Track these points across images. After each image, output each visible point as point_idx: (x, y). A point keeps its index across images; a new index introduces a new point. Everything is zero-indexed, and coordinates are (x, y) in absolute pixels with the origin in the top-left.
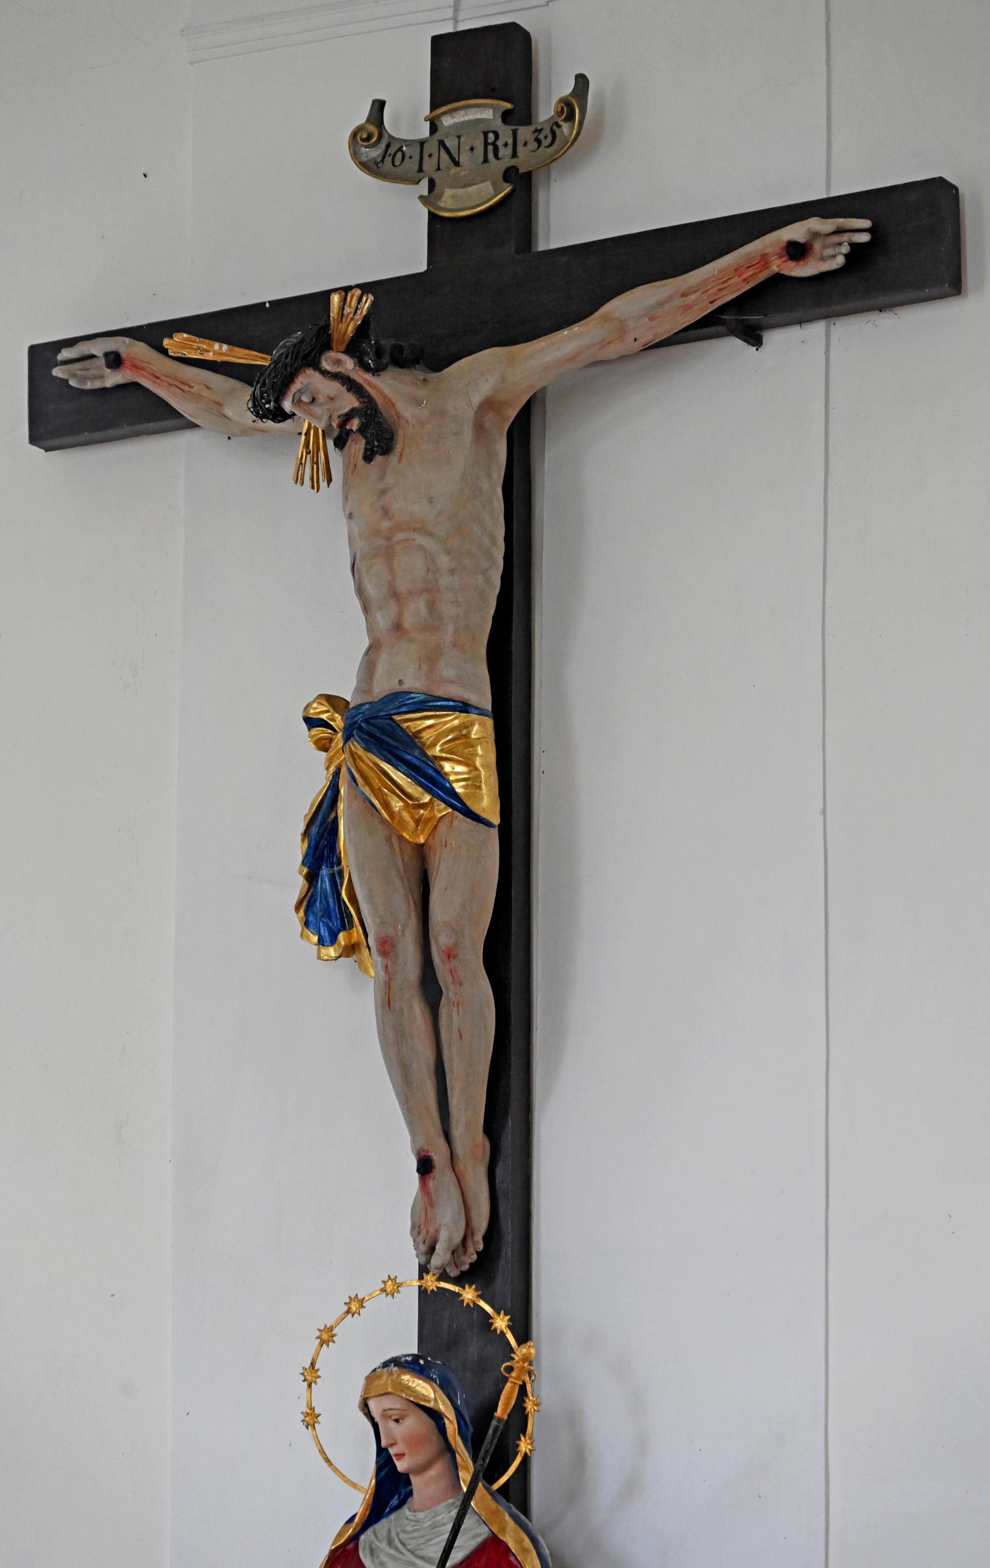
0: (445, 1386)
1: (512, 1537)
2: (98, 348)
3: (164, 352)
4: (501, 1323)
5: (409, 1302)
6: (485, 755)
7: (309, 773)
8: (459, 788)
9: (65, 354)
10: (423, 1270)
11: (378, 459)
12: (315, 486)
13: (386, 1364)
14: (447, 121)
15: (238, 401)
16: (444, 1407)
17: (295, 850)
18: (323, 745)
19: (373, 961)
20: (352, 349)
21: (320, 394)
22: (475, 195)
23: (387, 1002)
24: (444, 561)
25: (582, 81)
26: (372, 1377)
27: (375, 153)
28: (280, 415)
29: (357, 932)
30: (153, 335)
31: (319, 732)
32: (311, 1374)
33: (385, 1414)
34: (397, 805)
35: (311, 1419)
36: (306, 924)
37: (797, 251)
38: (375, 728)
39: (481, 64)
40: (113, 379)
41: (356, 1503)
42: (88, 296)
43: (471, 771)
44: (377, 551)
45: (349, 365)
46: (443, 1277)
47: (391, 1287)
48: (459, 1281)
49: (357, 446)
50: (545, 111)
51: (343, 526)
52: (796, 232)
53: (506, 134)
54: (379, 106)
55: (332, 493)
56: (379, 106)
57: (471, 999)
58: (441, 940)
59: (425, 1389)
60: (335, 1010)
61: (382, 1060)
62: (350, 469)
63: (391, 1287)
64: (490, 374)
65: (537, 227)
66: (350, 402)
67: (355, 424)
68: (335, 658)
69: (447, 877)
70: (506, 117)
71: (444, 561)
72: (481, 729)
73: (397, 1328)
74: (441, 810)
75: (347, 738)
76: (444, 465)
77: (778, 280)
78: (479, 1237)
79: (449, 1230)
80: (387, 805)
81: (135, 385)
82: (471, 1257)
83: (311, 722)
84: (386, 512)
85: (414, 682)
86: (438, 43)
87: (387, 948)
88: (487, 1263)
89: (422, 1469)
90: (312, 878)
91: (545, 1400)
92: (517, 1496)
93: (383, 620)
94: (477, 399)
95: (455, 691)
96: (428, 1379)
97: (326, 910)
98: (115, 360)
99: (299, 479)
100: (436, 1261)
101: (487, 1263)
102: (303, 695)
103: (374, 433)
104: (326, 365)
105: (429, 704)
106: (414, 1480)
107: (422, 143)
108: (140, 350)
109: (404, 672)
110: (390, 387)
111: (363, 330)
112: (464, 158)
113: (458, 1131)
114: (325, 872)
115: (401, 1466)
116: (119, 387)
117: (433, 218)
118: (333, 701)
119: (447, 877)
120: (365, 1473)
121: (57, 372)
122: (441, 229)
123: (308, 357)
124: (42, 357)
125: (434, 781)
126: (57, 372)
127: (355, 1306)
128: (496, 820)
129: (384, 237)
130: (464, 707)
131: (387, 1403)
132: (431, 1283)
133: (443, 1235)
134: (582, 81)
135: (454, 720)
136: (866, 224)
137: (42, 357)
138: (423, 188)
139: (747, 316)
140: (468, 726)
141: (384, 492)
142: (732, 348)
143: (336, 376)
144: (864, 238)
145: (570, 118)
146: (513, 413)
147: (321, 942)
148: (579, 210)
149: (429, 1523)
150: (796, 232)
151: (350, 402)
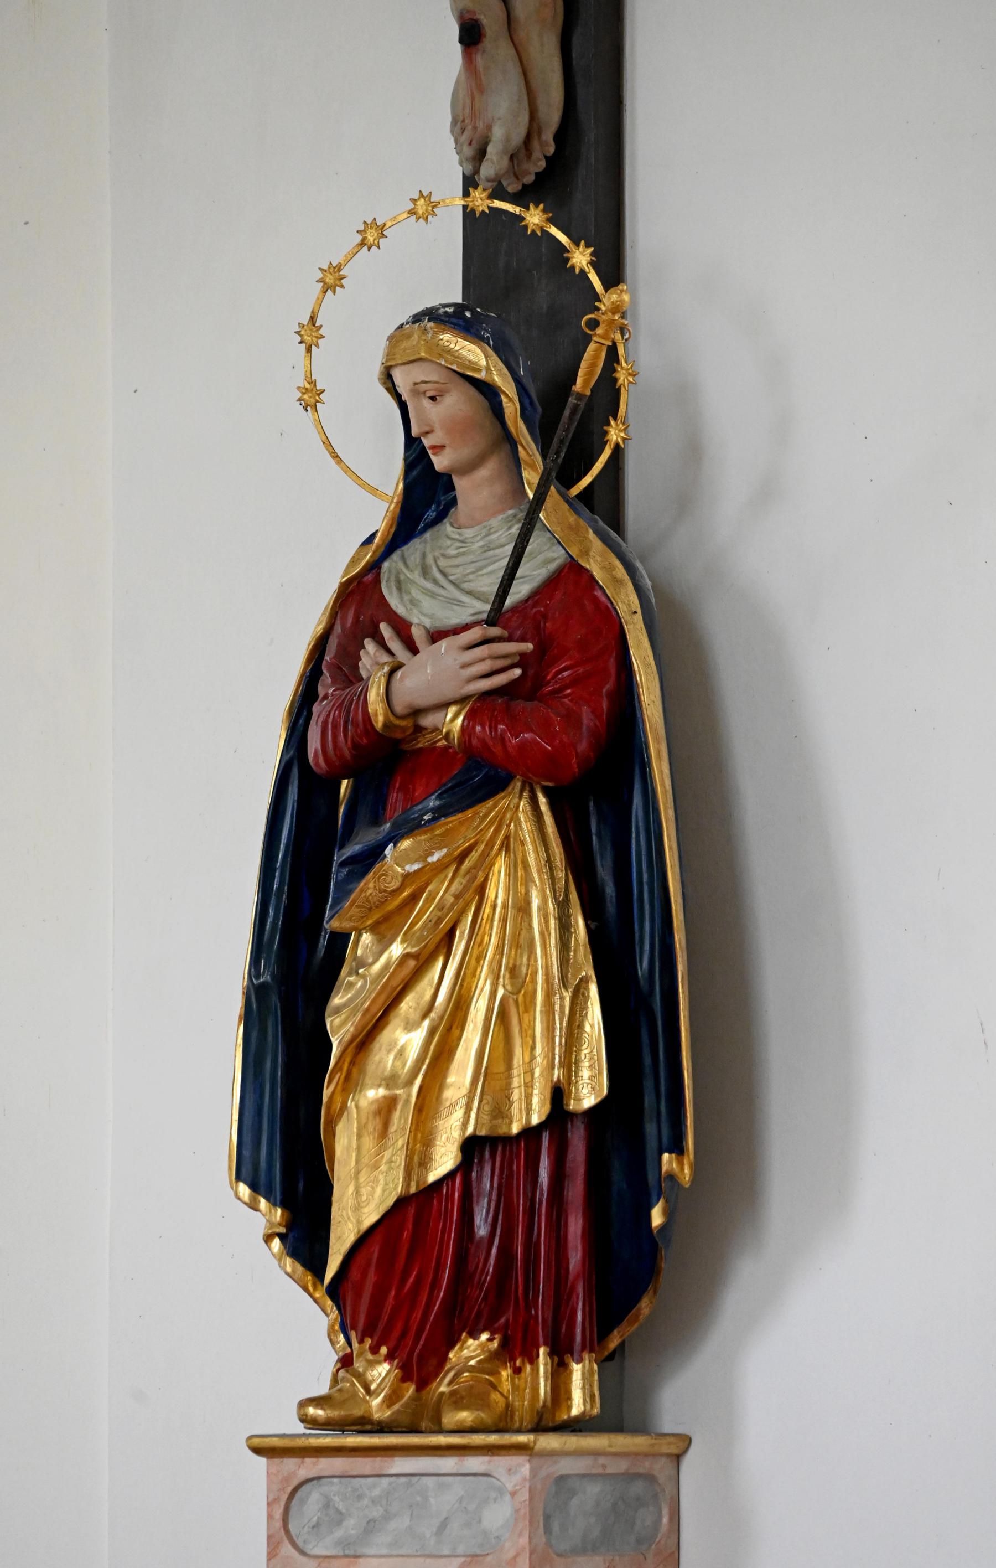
1: (599, 563)
10: (469, 183)
13: (417, 319)
16: (501, 379)
32: (310, 333)
35: (311, 397)
41: (376, 516)
46: (498, 193)
47: (422, 208)
48: (521, 198)
59: (473, 354)
63: (422, 208)
78: (548, 136)
79: (505, 121)
89: (469, 467)
91: (645, 369)
92: (605, 506)
100: (487, 170)
106: (461, 484)
115: (440, 462)
120: (389, 474)
127: (372, 235)
131: (419, 373)
132: (480, 201)
133: (498, 133)
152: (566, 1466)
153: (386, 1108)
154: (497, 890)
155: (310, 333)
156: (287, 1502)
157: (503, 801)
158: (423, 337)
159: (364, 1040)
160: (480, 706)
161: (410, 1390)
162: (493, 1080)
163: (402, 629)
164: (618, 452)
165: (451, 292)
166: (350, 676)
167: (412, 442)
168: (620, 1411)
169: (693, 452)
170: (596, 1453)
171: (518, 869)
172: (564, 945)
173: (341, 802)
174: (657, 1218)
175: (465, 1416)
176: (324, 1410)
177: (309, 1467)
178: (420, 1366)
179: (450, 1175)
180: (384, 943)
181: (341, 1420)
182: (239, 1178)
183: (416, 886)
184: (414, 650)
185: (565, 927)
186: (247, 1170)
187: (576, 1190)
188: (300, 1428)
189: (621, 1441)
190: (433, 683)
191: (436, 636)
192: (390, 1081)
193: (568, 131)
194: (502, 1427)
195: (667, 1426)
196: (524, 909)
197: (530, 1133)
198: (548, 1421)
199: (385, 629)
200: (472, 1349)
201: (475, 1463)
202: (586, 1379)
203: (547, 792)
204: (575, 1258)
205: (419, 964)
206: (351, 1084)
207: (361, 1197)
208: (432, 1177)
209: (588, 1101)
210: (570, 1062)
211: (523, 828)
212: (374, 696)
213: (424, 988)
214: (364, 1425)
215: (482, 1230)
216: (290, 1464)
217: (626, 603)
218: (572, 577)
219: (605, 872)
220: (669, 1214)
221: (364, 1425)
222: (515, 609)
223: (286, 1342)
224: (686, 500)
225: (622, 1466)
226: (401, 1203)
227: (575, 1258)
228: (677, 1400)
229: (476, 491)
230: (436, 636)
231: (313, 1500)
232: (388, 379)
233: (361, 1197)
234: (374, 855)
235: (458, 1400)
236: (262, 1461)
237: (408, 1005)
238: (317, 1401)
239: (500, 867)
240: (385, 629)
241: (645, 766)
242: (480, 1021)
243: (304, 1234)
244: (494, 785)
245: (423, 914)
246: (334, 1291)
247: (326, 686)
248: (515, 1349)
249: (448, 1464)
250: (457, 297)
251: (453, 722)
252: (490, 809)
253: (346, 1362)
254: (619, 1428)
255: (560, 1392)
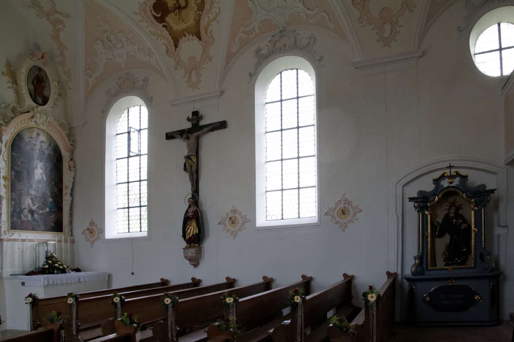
5: (191, 195)
7: (184, 161)
15: (179, 136)
21: (185, 135)
22: (195, 122)
23: (190, 175)
30: (174, 132)
38: (188, 157)
41: (187, 207)
42: (170, 130)
44: (188, 145)
57: (195, 175)
60: (186, 176)
64: (195, 134)
65: (29, 316)
68: (186, 153)
72: (195, 157)
73: (190, 196)
76: (192, 140)
79: (193, 189)
88: (196, 191)
91: (200, 200)
92: (198, 206)
97: (185, 169)
101: (196, 191)
103: (188, 138)
109: (190, 154)
120: (188, 205)
122: (193, 125)
124: (167, 134)
125: (192, 161)
129: (188, 125)
137: (167, 134)
139: (212, 130)
142: (212, 133)
148: (202, 123)
149: (69, 244)
156: (184, 251)
158: (198, 12)
162: (193, 232)
169: (202, 204)
173: (186, 220)
176: (218, 321)
178: (190, 245)
181: (186, 248)
190: (190, 214)
194: (194, 247)
207: (187, 237)
211: (194, 220)
218: (196, 210)
223: (184, 244)
224: (201, 206)
228: (201, 246)
233: (187, 237)
242: (193, 229)
243: (185, 239)
248: (194, 244)
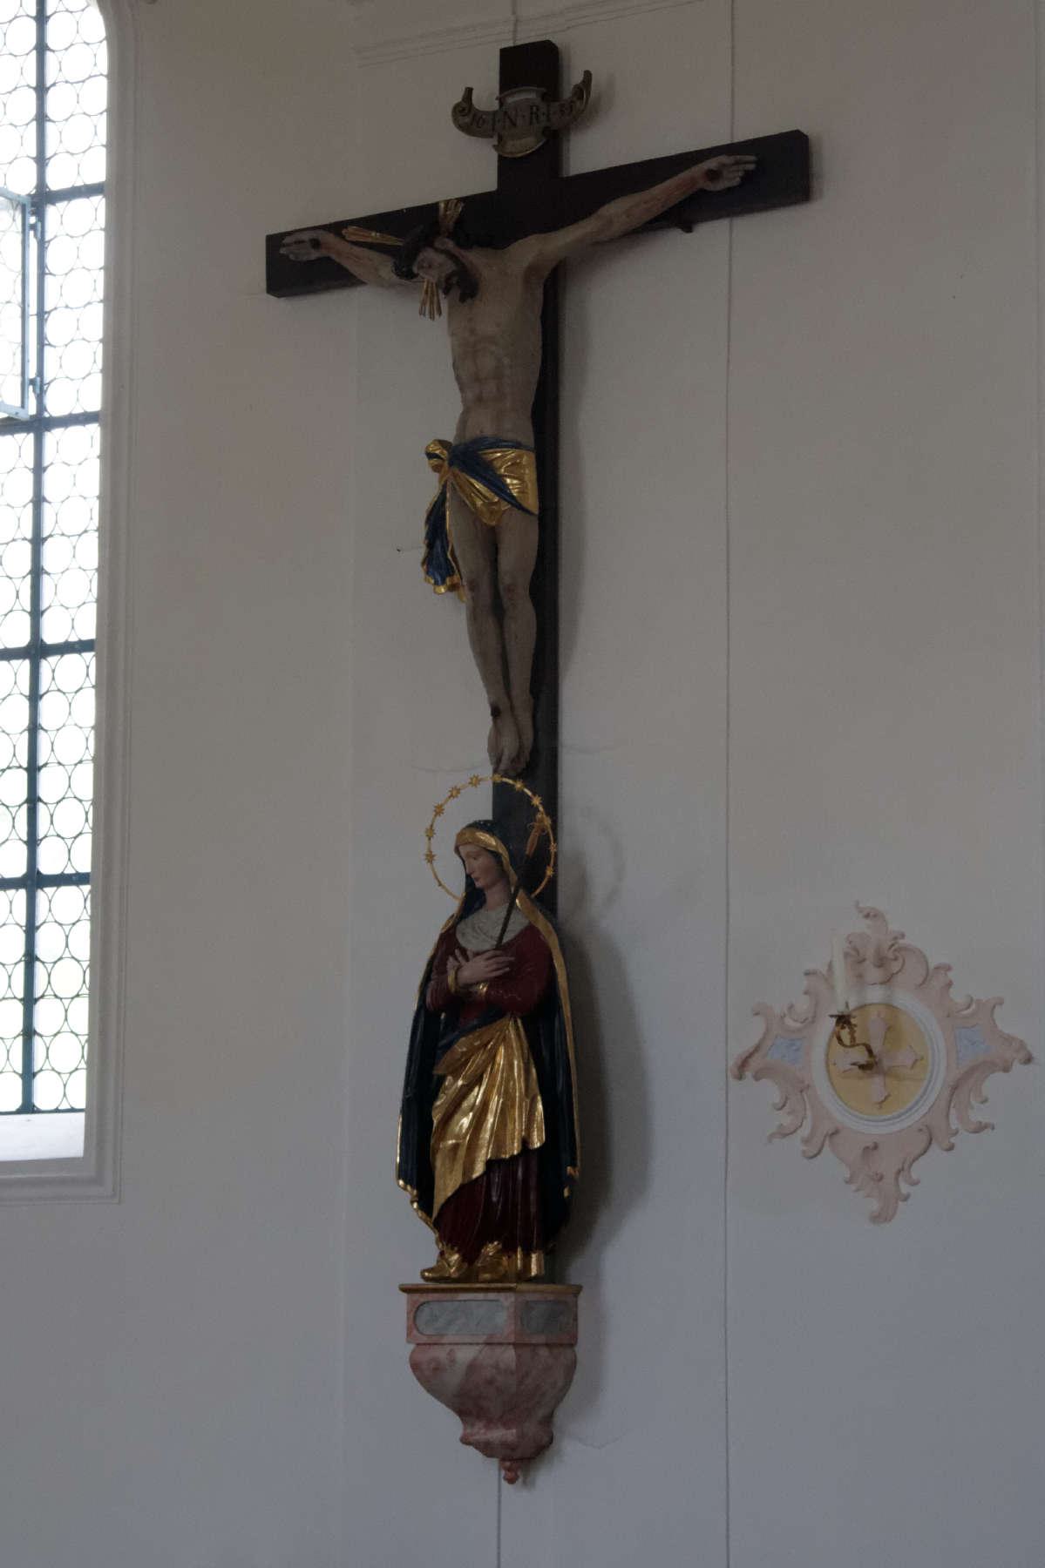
0: (504, 840)
1: (542, 924)
2: (306, 237)
3: (343, 237)
4: (536, 801)
6: (530, 474)
7: (428, 486)
8: (515, 493)
9: (287, 240)
10: (495, 771)
11: (469, 301)
12: (432, 317)
13: (470, 826)
14: (510, 100)
16: (502, 850)
17: (420, 531)
18: (436, 469)
19: (466, 593)
20: (452, 235)
21: (435, 265)
22: (524, 144)
23: (474, 617)
24: (506, 361)
25: (588, 75)
26: (460, 835)
27: (467, 120)
28: (410, 275)
29: (456, 578)
30: (337, 228)
31: (435, 461)
32: (430, 833)
33: (468, 855)
34: (479, 503)
35: (430, 857)
36: (427, 572)
37: (713, 175)
38: (464, 458)
39: (531, 65)
40: (314, 255)
41: (453, 906)
43: (521, 483)
44: (467, 354)
45: (450, 245)
46: (506, 775)
47: (475, 782)
48: (514, 779)
49: (456, 293)
50: (567, 92)
51: (458, 395)
52: (711, 164)
53: (543, 109)
54: (469, 91)
55: (443, 320)
56: (469, 91)
58: (505, 579)
59: (491, 841)
60: (445, 619)
61: (481, 683)
62: (450, 307)
63: (475, 782)
64: (531, 250)
66: (450, 267)
67: (454, 280)
69: (510, 565)
70: (544, 97)
71: (506, 361)
72: (528, 459)
73: (481, 806)
74: (505, 506)
75: (451, 465)
77: (702, 191)
78: (527, 752)
79: (509, 745)
80: (474, 504)
81: (329, 258)
82: (523, 765)
83: (430, 456)
84: (472, 331)
85: (489, 430)
86: (505, 53)
87: (473, 586)
89: (489, 887)
90: (430, 546)
91: (566, 844)
92: (547, 902)
93: (470, 395)
94: (525, 264)
95: (510, 436)
96: (493, 835)
97: (438, 563)
98: (316, 244)
99: (422, 313)
100: (502, 767)
101: (531, 759)
102: (426, 441)
103: (463, 287)
104: (437, 244)
105: (497, 444)
106: (488, 893)
107: (495, 113)
108: (330, 238)
109: (484, 425)
110: (475, 258)
111: (460, 222)
112: (519, 122)
113: (515, 692)
114: (438, 543)
115: (478, 884)
116: (319, 259)
117: (501, 159)
118: (443, 443)
119: (510, 565)
120: (459, 888)
121: (283, 251)
122: (506, 166)
123: (428, 241)
125: (498, 487)
126: (283, 251)
127: (455, 792)
128: (536, 511)
129: (471, 170)
130: (517, 445)
131: (469, 848)
132: (498, 779)
133: (506, 752)
134: (588, 75)
135: (511, 454)
136: (752, 158)
138: (495, 141)
140: (520, 457)
141: (470, 320)
142: (676, 237)
143: (442, 252)
144: (751, 167)
145: (581, 98)
146: (546, 274)
147: (436, 583)
148: (589, 152)
150: (711, 164)
151: (450, 267)
152: (530, 1297)
153: (456, 1147)
154: (500, 1060)
155: (430, 833)
156: (415, 1312)
157: (504, 1021)
159: (448, 1117)
160: (493, 983)
161: (466, 1265)
163: (464, 951)
164: (553, 882)
165: (486, 814)
166: (443, 972)
167: (468, 876)
168: (552, 1274)
169: (583, 881)
170: (542, 1292)
171: (508, 1048)
172: (527, 1080)
173: (444, 1023)
174: (566, 1193)
175: (487, 1276)
177: (422, 1298)
179: (481, 1176)
180: (456, 1080)
181: (437, 1283)
182: (399, 1177)
183: (467, 1057)
184: (467, 959)
185: (527, 1072)
186: (403, 1173)
187: (533, 1182)
188: (422, 1281)
189: (551, 1287)
190: (475, 972)
191: (477, 954)
192: (457, 1137)
193: (535, 751)
194: (503, 1281)
195: (574, 1281)
196: (511, 1066)
197: (513, 1158)
198: (523, 1276)
199: (457, 952)
200: (491, 1249)
201: (492, 1296)
202: (538, 1260)
203: (523, 1019)
204: (533, 1209)
205: (468, 1088)
206: (442, 1138)
207: (447, 1184)
208: (475, 1176)
209: (537, 1145)
210: (529, 1129)
211: (512, 1030)
212: (450, 979)
213: (471, 1098)
214: (447, 1280)
215: (494, 1199)
216: (416, 1297)
217: (553, 942)
218: (530, 931)
219: (545, 1053)
220: (571, 1191)
221: (447, 1280)
222: (510, 944)
223: (418, 1247)
224: (581, 897)
225: (551, 1297)
226: (462, 1187)
227: (533, 1209)
228: (576, 1271)
229: (495, 896)
230: (477, 954)
231: (426, 1309)
232: (457, 850)
233: (447, 1184)
234: (449, 1045)
235: (484, 1269)
236: (404, 1296)
237: (465, 1104)
238: (429, 1270)
239: (502, 1050)
240: (457, 952)
241: (560, 1007)
242: (495, 1111)
243: (425, 1200)
244: (500, 1015)
245: (470, 1068)
246: (437, 1225)
247: (434, 976)
248: (508, 1249)
249: (481, 1296)
250: (489, 816)
251: (483, 988)
252: (498, 1025)
253: (442, 1254)
254: (553, 1282)
255: (527, 1266)
